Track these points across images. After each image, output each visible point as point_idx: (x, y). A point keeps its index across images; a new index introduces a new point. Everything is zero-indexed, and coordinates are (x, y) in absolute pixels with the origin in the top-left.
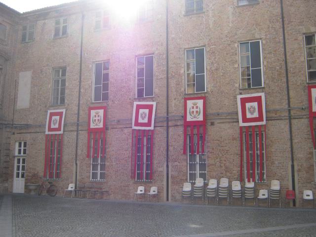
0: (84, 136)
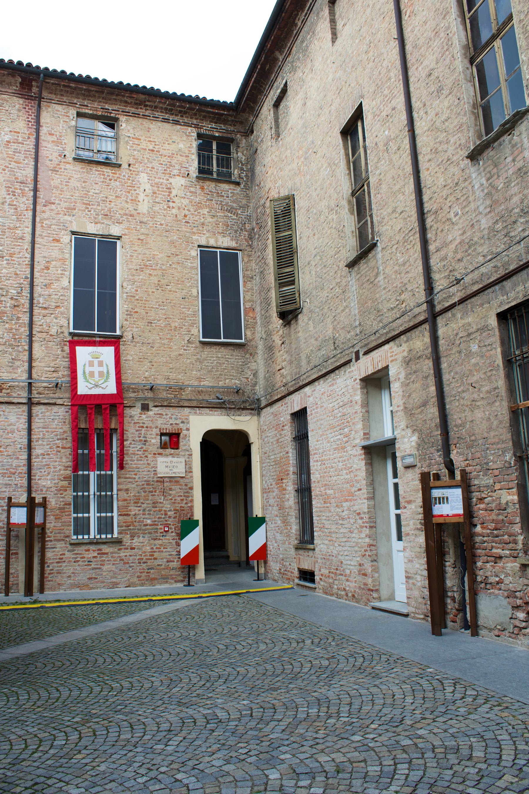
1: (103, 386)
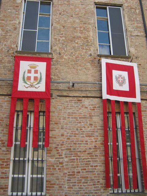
1: (37, 86)
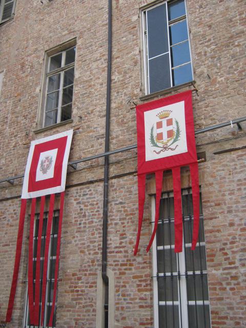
0: (126, 191)
1: (173, 146)
